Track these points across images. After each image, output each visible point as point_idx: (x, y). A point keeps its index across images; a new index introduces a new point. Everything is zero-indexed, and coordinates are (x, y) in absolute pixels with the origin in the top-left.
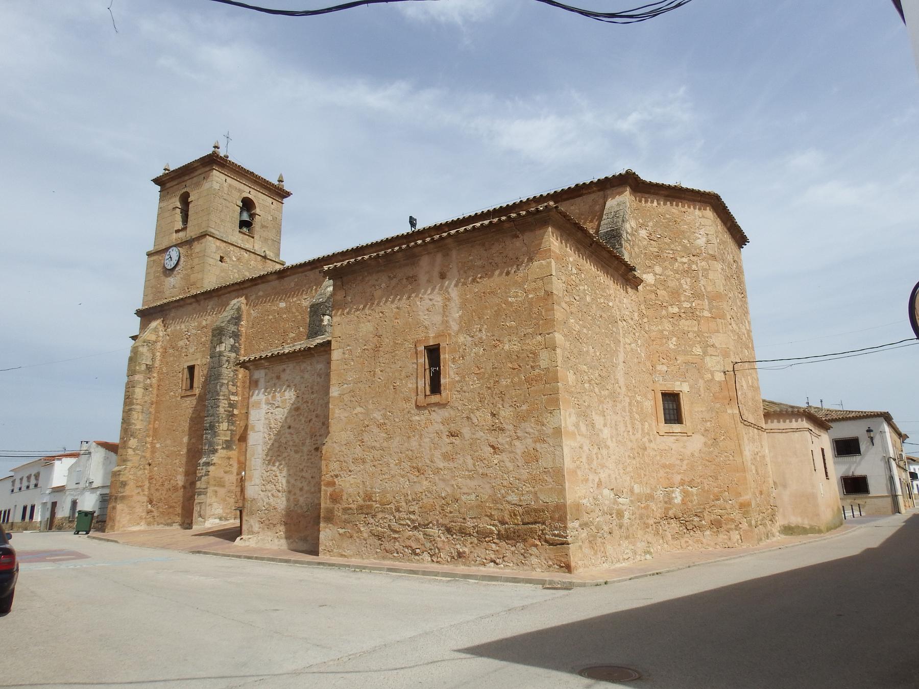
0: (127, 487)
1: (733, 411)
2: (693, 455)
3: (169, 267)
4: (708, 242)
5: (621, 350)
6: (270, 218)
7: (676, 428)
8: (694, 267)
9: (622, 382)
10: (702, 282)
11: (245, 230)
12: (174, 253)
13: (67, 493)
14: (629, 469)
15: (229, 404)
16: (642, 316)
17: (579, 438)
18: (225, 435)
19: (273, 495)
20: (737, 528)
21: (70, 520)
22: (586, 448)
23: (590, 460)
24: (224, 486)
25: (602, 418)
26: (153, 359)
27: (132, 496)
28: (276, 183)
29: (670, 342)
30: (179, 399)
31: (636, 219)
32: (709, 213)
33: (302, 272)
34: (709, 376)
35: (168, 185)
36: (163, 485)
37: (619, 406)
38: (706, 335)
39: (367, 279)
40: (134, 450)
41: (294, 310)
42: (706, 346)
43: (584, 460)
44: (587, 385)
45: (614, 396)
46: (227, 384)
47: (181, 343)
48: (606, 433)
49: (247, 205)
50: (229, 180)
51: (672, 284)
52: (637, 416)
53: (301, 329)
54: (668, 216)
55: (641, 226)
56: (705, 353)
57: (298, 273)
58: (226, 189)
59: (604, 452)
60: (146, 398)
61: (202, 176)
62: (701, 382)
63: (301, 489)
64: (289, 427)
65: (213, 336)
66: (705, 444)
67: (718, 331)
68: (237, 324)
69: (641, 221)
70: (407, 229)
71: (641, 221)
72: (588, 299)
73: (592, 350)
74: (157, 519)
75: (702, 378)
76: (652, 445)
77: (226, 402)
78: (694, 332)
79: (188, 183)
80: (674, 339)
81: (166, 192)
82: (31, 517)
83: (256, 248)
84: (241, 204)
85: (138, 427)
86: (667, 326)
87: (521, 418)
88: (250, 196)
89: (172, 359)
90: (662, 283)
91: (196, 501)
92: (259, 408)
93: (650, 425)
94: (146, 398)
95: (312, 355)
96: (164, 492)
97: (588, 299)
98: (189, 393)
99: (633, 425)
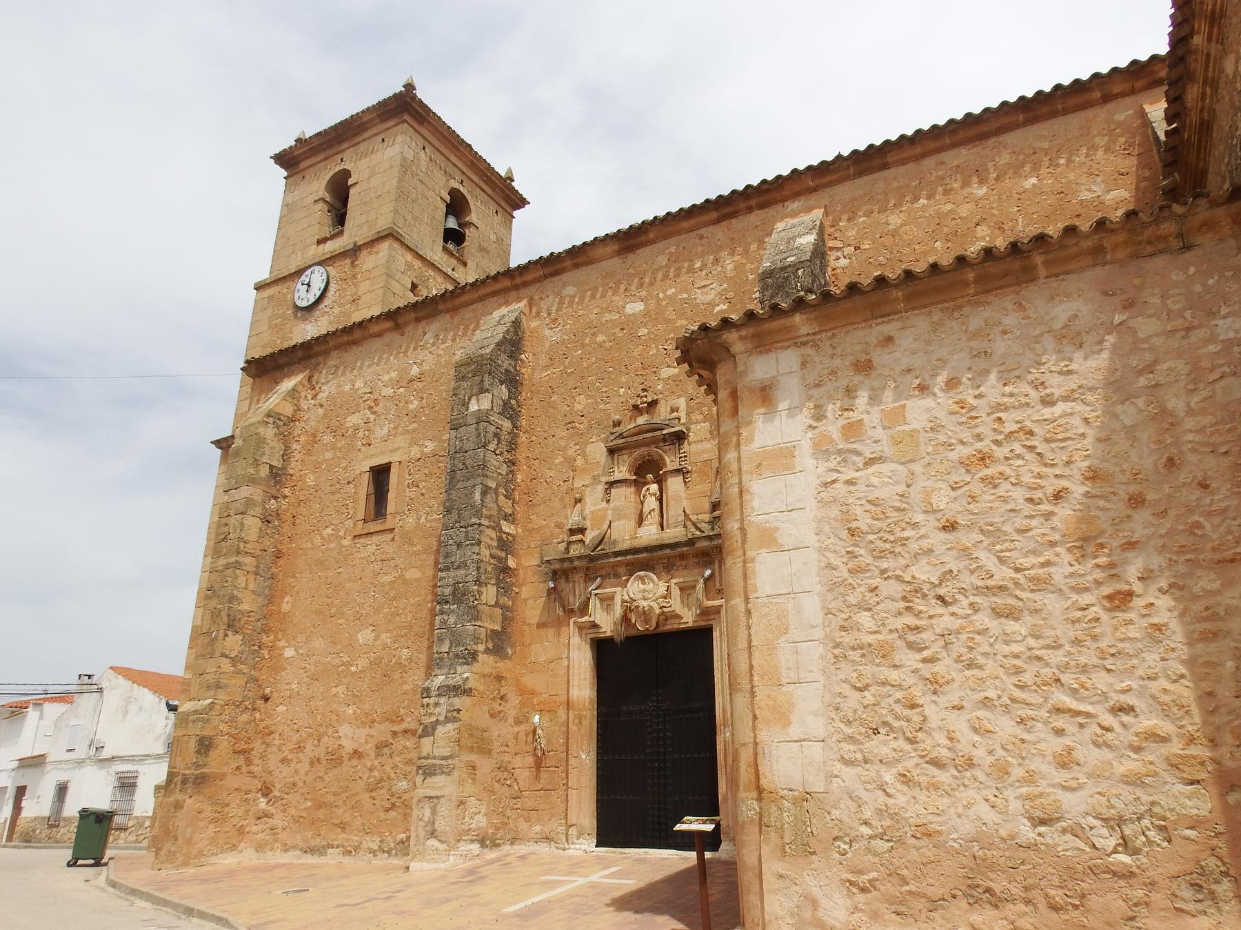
0: (213, 754)
3: (304, 304)
11: (451, 246)
12: (317, 278)
13: (48, 767)
15: (500, 540)
18: (491, 618)
19: (905, 778)
21: (54, 822)
24: (489, 752)
26: (286, 456)
27: (222, 777)
30: (346, 542)
33: (690, 230)
36: (300, 748)
40: (234, 661)
41: (670, 314)
47: (354, 420)
49: (457, 205)
57: (678, 233)
60: (267, 542)
61: (379, 138)
63: (1065, 761)
65: (460, 378)
68: (514, 356)
74: (283, 836)
77: (493, 535)
79: (346, 155)
84: (448, 198)
85: (245, 607)
89: (329, 455)
92: (789, 469)
94: (267, 542)
95: (1027, 276)
96: (304, 767)
98: (373, 527)
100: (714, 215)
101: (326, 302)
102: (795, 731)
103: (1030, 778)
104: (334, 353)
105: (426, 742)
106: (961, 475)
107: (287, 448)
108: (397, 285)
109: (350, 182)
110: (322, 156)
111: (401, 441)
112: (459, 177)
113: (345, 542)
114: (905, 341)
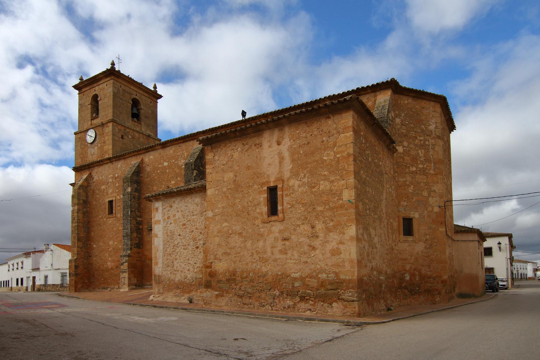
1: (442, 229)
2: (418, 253)
4: (436, 127)
5: (385, 191)
6: (150, 112)
7: (410, 238)
8: (427, 143)
9: (384, 211)
10: (431, 153)
14: (386, 261)
15: (137, 222)
16: (395, 172)
17: (363, 242)
20: (439, 294)
22: (366, 248)
23: (368, 255)
25: (374, 231)
26: (87, 196)
28: (153, 89)
29: (409, 188)
31: (395, 112)
32: (438, 109)
33: (177, 144)
34: (431, 209)
35: (83, 90)
37: (382, 225)
38: (431, 184)
39: (228, 145)
42: (430, 192)
43: (365, 254)
44: (368, 211)
45: (380, 219)
46: (135, 211)
48: (376, 240)
49: (135, 103)
50: (123, 86)
51: (413, 153)
52: (390, 231)
53: (179, 179)
54: (413, 110)
55: (396, 116)
56: (429, 195)
58: (121, 92)
59: (375, 250)
62: (426, 212)
63: (189, 270)
64: (180, 235)
65: (124, 183)
66: (425, 248)
67: (438, 183)
69: (397, 112)
70: (240, 118)
71: (397, 112)
72: (370, 159)
73: (371, 191)
75: (427, 210)
76: (396, 248)
78: (424, 183)
80: (412, 186)
81: (82, 94)
82: (22, 284)
83: (143, 130)
86: (409, 178)
87: (329, 230)
88: (137, 97)
90: (406, 152)
91: (121, 276)
93: (396, 236)
95: (192, 193)
97: (370, 159)
99: (388, 235)
100: (182, 141)
101: (97, 139)
102: (159, 266)
103: (185, 273)
104: (96, 167)
105: (122, 266)
106: (181, 227)
107: (87, 194)
108: (116, 137)
109: (99, 99)
110: (88, 88)
111: (115, 194)
112: (135, 93)
113: (104, 220)
114: (177, 202)
